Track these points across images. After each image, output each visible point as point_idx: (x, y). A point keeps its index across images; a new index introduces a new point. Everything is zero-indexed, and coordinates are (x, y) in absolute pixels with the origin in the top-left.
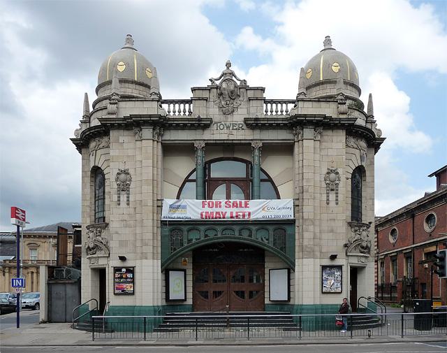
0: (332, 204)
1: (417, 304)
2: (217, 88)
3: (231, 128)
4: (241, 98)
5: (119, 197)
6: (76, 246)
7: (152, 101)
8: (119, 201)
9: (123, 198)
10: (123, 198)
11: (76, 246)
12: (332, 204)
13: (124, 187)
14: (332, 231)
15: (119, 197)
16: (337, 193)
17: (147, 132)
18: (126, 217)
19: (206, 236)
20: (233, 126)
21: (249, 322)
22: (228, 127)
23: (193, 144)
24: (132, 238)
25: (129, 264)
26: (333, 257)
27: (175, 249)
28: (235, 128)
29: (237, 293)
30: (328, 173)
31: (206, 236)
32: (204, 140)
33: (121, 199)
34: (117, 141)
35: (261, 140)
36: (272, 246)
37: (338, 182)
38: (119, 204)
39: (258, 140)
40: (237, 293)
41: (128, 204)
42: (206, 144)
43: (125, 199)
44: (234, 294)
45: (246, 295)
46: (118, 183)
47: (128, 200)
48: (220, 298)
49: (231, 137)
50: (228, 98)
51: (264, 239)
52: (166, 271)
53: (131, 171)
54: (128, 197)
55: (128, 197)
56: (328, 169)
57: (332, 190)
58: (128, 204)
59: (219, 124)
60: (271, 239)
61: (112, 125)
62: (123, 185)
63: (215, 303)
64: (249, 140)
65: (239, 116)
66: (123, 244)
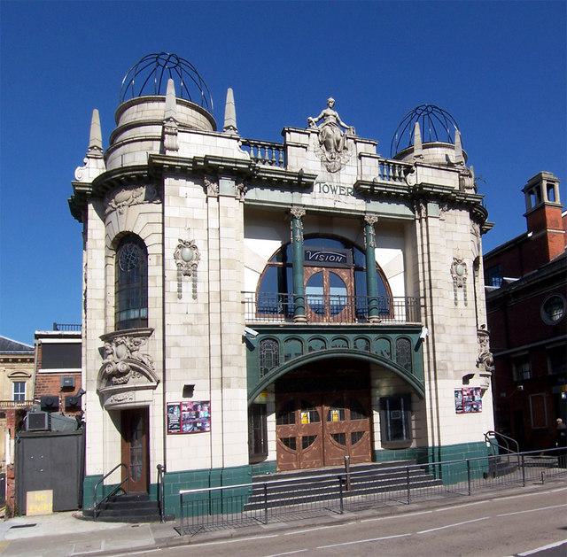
0: (461, 304)
1: (562, 434)
2: (318, 133)
3: (338, 192)
4: (349, 152)
5: (180, 286)
6: (41, 371)
7: (231, 138)
8: (180, 291)
9: (187, 287)
10: (187, 287)
11: (41, 371)
12: (461, 304)
13: (188, 270)
14: (463, 342)
15: (180, 286)
16: (195, 281)
17: (227, 185)
18: (190, 319)
19: (311, 349)
20: (340, 190)
21: (408, 481)
22: (334, 191)
23: (364, 217)
24: (204, 355)
25: (198, 396)
26: (466, 379)
27: (266, 371)
28: (342, 192)
29: (336, 436)
30: (179, 247)
31: (311, 349)
32: (304, 206)
33: (184, 288)
34: (176, 194)
35: (376, 213)
36: (395, 361)
37: (196, 262)
38: (180, 297)
39: (373, 212)
40: (336, 436)
41: (195, 297)
42: (307, 211)
43: (191, 289)
44: (331, 438)
45: (348, 440)
46: (179, 261)
47: (195, 291)
48: (313, 447)
49: (338, 206)
50: (333, 150)
51: (384, 353)
52: (256, 413)
53: (200, 244)
54: (195, 286)
55: (195, 286)
56: (454, 258)
57: (461, 286)
58: (195, 297)
59: (322, 185)
60: (394, 353)
61: (172, 168)
62: (187, 266)
63: (307, 456)
64: (362, 212)
65: (348, 177)
66: (187, 364)
